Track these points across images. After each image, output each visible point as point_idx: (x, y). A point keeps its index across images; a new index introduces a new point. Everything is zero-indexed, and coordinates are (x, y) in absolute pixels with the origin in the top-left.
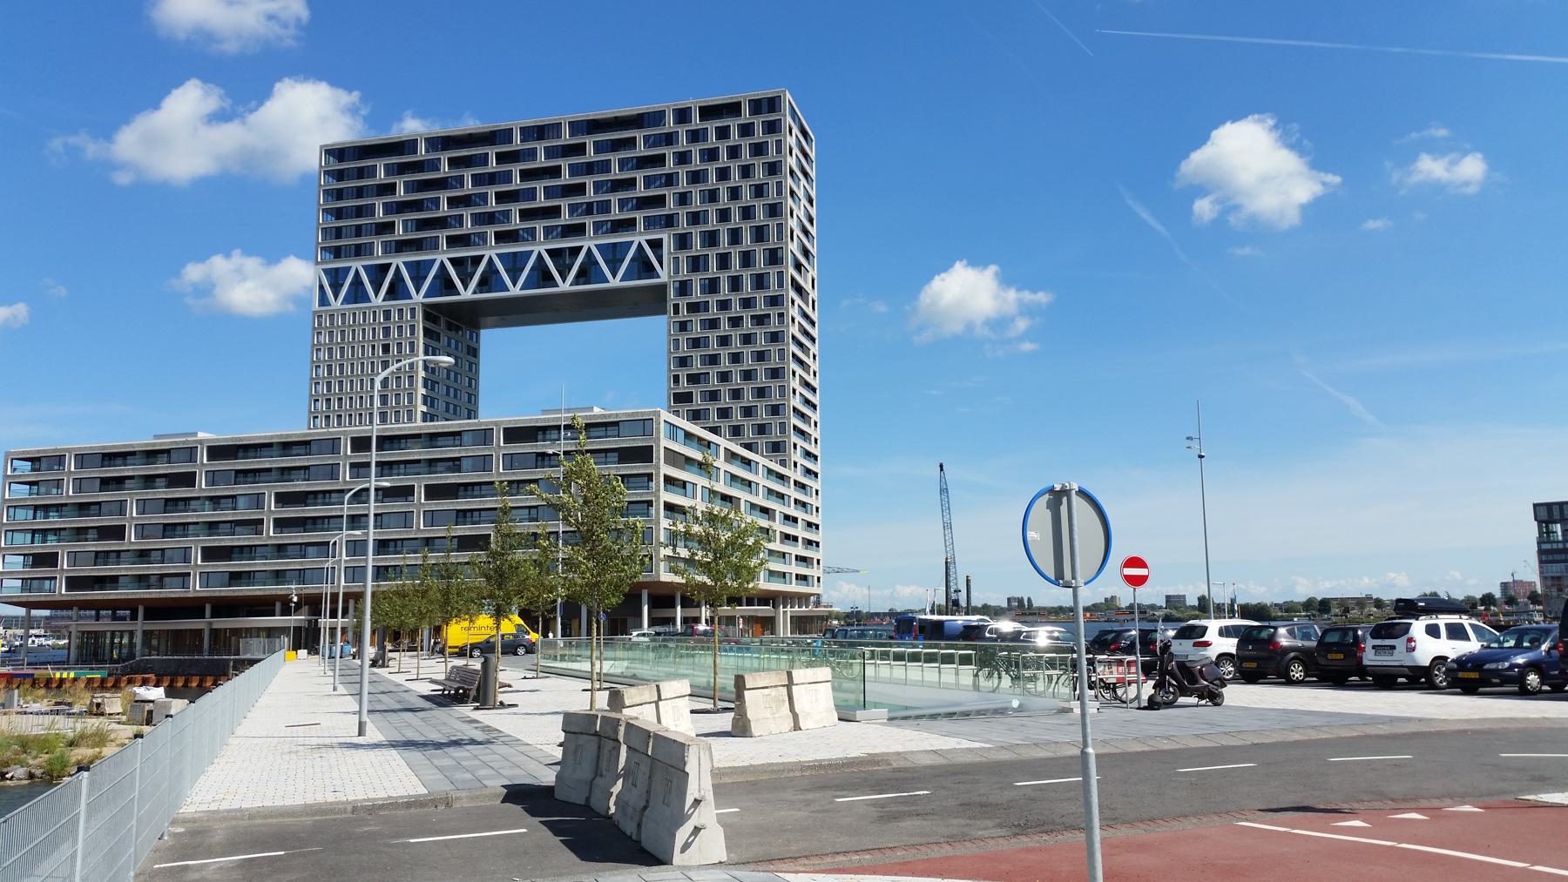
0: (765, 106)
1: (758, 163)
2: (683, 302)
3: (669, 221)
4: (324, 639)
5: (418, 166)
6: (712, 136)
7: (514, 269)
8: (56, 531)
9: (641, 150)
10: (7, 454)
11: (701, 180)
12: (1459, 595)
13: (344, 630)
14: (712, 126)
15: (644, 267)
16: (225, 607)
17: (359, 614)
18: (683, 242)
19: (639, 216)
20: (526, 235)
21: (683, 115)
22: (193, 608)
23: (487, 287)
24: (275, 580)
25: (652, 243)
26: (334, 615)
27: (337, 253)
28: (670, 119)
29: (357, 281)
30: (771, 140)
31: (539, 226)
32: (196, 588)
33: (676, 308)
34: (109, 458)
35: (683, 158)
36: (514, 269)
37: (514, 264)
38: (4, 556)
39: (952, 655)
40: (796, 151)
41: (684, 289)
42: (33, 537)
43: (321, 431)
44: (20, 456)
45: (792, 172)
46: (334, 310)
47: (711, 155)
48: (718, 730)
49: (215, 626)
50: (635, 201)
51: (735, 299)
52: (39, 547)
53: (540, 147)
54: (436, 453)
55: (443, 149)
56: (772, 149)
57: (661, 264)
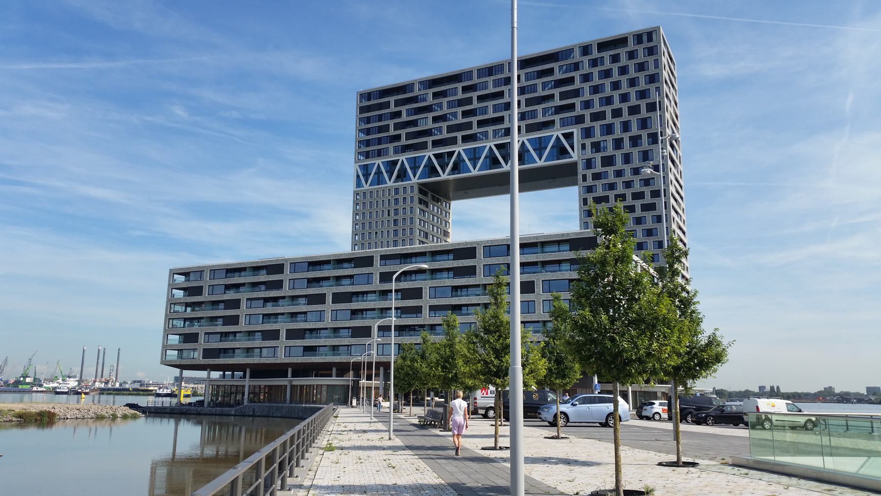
0: (645, 38)
1: (642, 76)
2: (589, 173)
3: (580, 120)
4: (363, 394)
5: (414, 100)
6: (607, 61)
7: (474, 160)
8: (199, 319)
9: (558, 75)
10: (171, 270)
11: (600, 91)
12: (813, 390)
13: (377, 388)
14: (607, 55)
15: (562, 152)
16: (302, 370)
17: (387, 377)
18: (588, 133)
19: (557, 118)
20: (481, 137)
21: (586, 50)
22: (279, 370)
23: (457, 171)
24: (332, 352)
25: (566, 136)
26: (369, 378)
27: (367, 155)
28: (577, 53)
29: (379, 172)
30: (651, 60)
31: (490, 129)
32: (281, 358)
33: (584, 178)
34: (232, 271)
35: (586, 78)
36: (474, 160)
37: (474, 156)
38: (168, 335)
39: (113, 391)
40: (667, 67)
41: (589, 164)
42: (185, 323)
43: (359, 252)
44: (178, 272)
45: (666, 81)
46: (365, 190)
47: (607, 74)
48: (85, 359)
49: (294, 383)
50: (553, 109)
51: (627, 168)
52: (187, 330)
53: (490, 80)
54: (437, 265)
55: (430, 88)
56: (651, 66)
57: (572, 148)
